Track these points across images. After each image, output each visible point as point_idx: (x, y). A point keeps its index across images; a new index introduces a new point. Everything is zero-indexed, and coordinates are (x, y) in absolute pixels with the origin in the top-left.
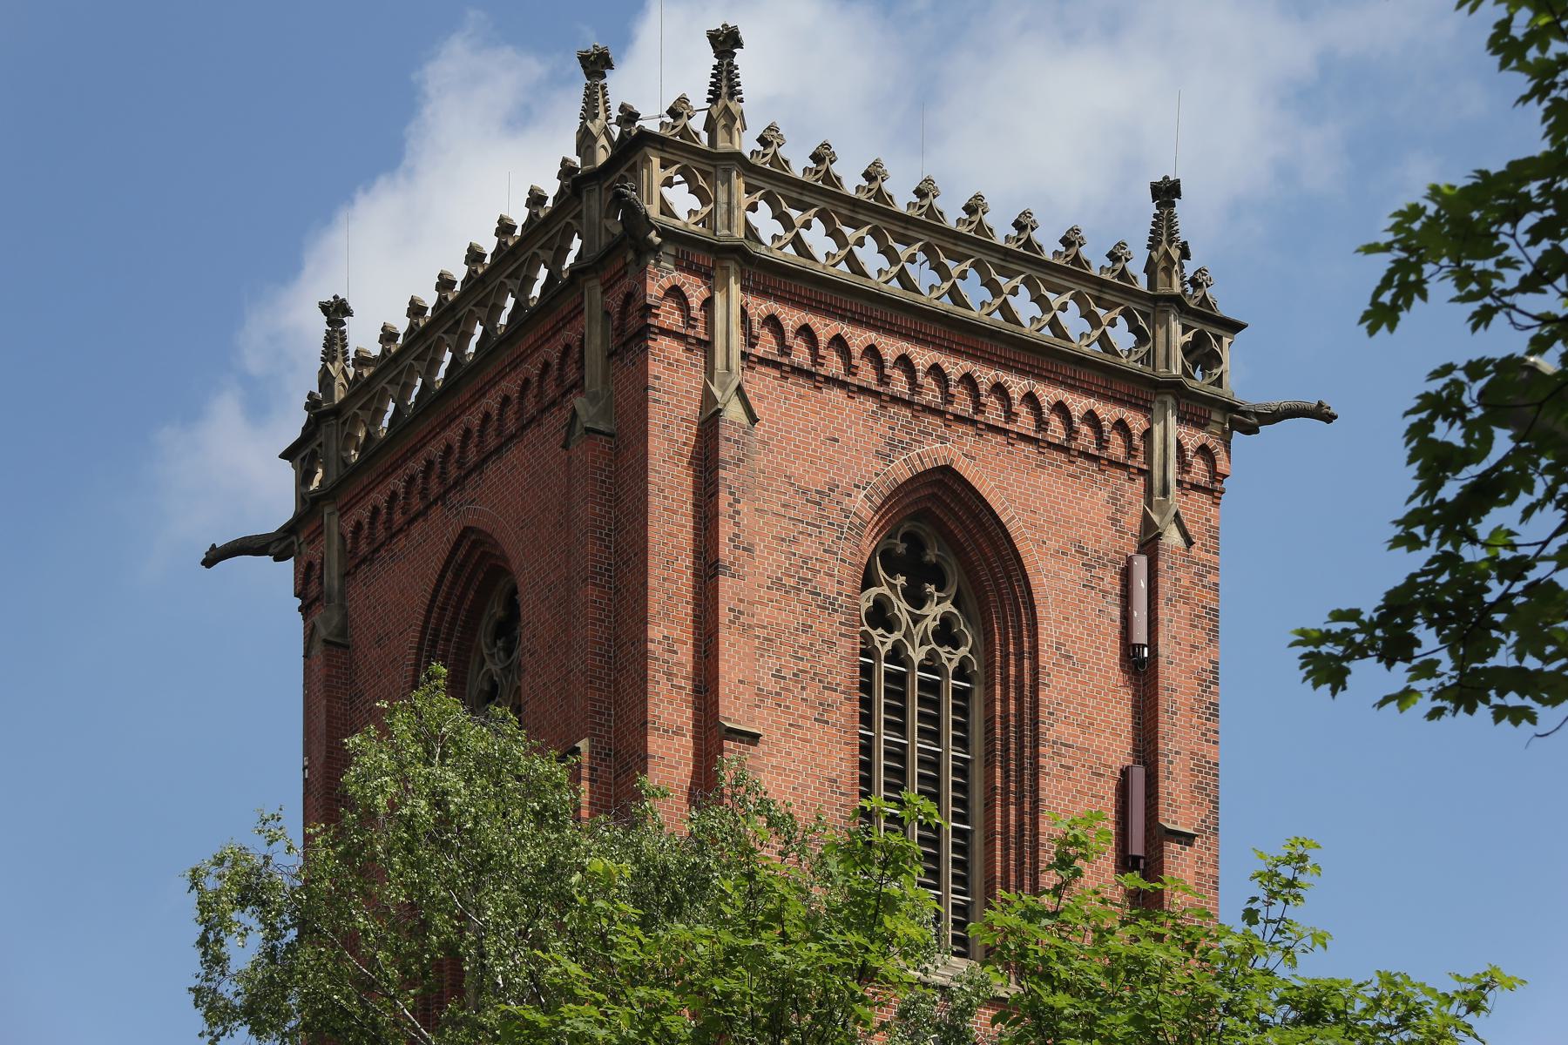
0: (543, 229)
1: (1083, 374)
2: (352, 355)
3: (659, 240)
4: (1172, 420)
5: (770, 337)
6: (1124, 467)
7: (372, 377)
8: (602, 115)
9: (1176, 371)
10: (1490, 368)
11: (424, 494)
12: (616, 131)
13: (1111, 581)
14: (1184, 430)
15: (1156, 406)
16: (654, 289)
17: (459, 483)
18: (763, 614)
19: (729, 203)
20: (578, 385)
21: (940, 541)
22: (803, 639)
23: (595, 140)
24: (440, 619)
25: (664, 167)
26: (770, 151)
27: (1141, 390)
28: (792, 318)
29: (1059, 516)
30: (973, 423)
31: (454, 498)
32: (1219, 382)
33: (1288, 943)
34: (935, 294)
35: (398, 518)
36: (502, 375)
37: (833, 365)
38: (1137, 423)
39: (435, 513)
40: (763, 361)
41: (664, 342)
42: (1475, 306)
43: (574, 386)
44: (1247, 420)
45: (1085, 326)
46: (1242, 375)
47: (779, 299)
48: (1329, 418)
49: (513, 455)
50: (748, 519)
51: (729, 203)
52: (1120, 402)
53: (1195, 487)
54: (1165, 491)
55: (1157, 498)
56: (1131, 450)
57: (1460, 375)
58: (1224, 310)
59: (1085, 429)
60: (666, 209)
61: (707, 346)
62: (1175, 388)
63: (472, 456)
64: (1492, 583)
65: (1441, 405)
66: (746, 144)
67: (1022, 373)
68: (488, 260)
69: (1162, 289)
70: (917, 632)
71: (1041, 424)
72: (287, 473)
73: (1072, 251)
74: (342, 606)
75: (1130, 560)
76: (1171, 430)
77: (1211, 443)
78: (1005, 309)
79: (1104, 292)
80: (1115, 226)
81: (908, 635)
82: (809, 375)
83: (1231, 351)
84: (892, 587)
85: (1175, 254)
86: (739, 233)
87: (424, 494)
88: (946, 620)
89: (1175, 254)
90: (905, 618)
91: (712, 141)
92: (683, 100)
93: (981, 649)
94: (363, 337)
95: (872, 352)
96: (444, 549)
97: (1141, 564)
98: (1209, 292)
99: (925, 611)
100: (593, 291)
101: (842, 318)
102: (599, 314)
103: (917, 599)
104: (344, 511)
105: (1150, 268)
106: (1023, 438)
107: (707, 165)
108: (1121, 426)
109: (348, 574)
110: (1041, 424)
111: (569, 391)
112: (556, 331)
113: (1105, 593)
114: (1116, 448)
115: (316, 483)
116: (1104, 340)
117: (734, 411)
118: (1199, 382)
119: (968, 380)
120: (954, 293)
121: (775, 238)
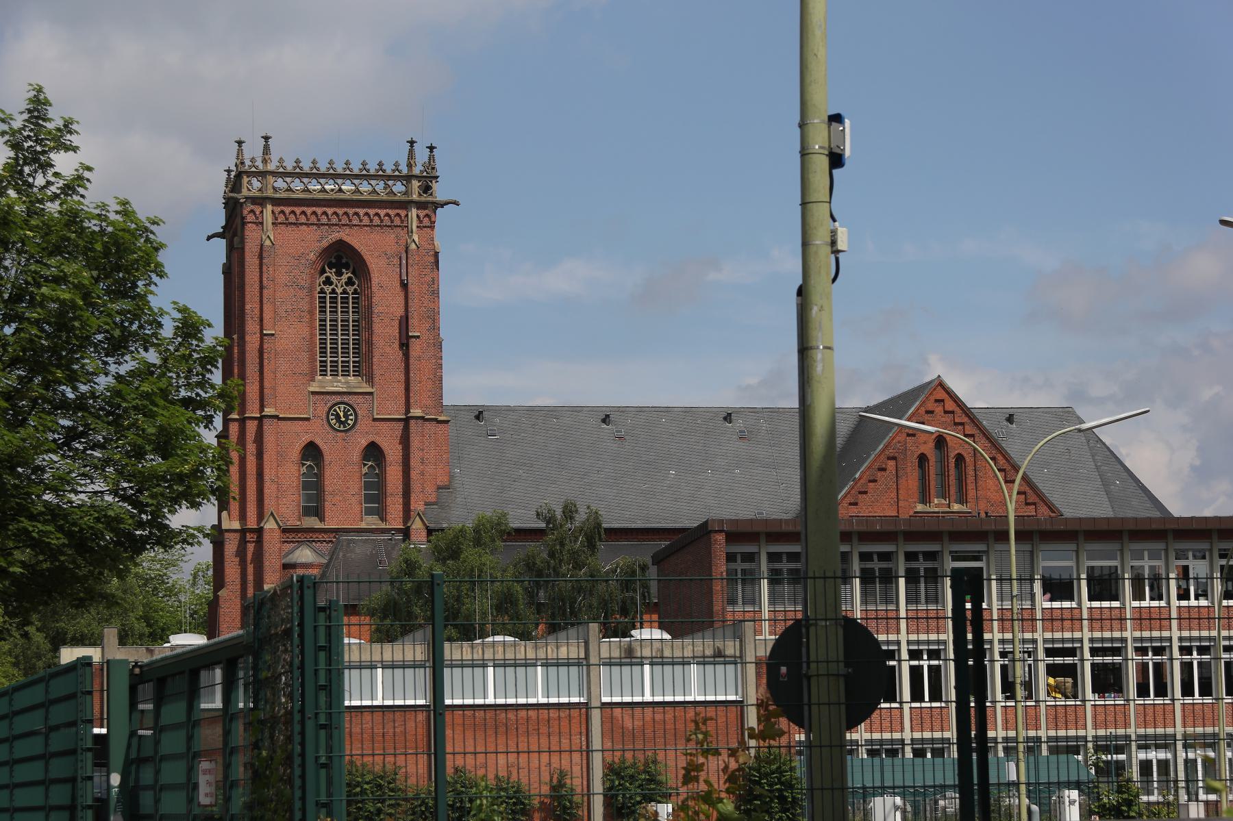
13: (396, 261)
21: (341, 258)
46: (440, 191)
56: (402, 222)
61: (262, 223)
88: (349, 278)
97: (404, 256)
103: (339, 274)
108: (398, 215)
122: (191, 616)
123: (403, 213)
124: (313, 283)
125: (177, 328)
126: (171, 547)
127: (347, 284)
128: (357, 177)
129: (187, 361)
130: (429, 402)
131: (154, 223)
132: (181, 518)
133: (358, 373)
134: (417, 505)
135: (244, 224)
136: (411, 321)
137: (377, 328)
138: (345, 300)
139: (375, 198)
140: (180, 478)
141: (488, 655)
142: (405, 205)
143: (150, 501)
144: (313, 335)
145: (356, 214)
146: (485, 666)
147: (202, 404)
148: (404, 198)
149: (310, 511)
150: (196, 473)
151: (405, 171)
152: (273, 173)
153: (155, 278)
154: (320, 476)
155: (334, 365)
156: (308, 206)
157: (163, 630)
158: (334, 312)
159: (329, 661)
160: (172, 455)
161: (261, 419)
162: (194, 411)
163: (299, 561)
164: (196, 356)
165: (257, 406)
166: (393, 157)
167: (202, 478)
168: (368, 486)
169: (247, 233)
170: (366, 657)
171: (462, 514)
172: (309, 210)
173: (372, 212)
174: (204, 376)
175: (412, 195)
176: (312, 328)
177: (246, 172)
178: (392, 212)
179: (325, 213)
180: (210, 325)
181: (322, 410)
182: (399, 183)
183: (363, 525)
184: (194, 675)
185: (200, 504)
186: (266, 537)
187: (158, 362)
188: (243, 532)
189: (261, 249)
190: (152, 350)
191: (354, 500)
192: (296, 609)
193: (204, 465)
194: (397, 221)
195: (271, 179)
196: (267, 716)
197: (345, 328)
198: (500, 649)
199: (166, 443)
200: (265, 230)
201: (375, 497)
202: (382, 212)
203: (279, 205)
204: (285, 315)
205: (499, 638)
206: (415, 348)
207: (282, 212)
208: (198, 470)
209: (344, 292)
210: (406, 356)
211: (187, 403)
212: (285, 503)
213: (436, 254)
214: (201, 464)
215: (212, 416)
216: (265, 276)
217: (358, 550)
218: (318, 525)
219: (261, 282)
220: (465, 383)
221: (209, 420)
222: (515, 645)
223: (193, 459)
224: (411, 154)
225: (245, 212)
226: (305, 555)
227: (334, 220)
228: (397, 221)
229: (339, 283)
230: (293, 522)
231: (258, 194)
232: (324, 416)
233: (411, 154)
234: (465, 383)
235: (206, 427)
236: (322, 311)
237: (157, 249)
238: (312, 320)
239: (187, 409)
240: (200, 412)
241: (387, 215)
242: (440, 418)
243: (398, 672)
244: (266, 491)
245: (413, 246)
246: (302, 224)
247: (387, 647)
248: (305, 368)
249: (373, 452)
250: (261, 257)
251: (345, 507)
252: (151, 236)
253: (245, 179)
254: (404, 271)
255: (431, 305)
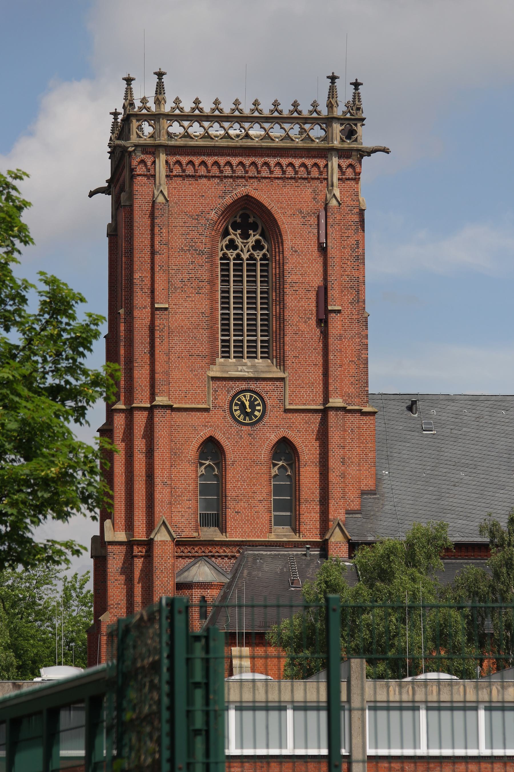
13: (313, 220)
15: (329, 156)
21: (248, 217)
29: (285, 201)
41: (140, 178)
46: (366, 138)
48: (388, 153)
56: (321, 173)
61: (154, 176)
77: (353, 162)
81: (242, 250)
84: (236, 235)
88: (258, 242)
97: (322, 214)
99: (249, 240)
101: (204, 155)
103: (245, 236)
106: (278, 178)
108: (316, 165)
113: (311, 225)
122: (67, 644)
123: (322, 163)
124: (213, 248)
125: (44, 303)
126: (34, 566)
127: (254, 248)
128: (267, 119)
129: (55, 342)
130: (352, 390)
131: (16, 177)
132: (46, 531)
133: (266, 355)
134: (337, 514)
135: (132, 177)
136: (330, 293)
137: (290, 301)
138: (252, 267)
139: (288, 144)
140: (46, 482)
141: (420, 696)
142: (324, 153)
143: (10, 511)
144: (213, 309)
145: (266, 164)
146: (415, 709)
147: (73, 394)
148: (323, 145)
149: (206, 521)
150: (65, 478)
151: (324, 112)
152: (171, 117)
153: (18, 244)
154: (221, 478)
155: (239, 344)
156: (209, 155)
157: (34, 662)
158: (239, 281)
159: (207, 701)
160: (36, 456)
161: (151, 410)
162: (63, 402)
163: (196, 580)
164: (65, 336)
165: (147, 393)
166: (311, 95)
167: (72, 483)
168: (278, 490)
169: (136, 188)
170: (273, 696)
171: (392, 526)
172: (209, 161)
173: (284, 161)
174: (75, 360)
175: (331, 140)
176: (213, 300)
177: (136, 115)
178: (309, 162)
179: (229, 163)
180: (82, 300)
181: (224, 399)
182: (317, 127)
183: (272, 538)
184: (53, 715)
185: (68, 514)
186: (157, 551)
187: (21, 344)
188: (130, 544)
189: (153, 206)
190: (14, 330)
191: (261, 508)
192: (165, 638)
193: (74, 468)
194: (315, 173)
195: (165, 123)
196: (132, 766)
197: (252, 301)
198: (435, 689)
199: (29, 440)
200: (157, 183)
201: (287, 504)
202: (297, 162)
203: (175, 154)
204: (180, 285)
205: (432, 676)
206: (336, 324)
207: (178, 162)
208: (66, 474)
209: (251, 258)
210: (325, 335)
211: (54, 392)
212: (179, 511)
213: (361, 212)
214: (70, 467)
215: (84, 408)
216: (157, 239)
217: (266, 568)
218: (219, 537)
219: (152, 246)
220: (393, 368)
221: (80, 413)
222: (450, 684)
223: (60, 460)
224: (332, 92)
225: (134, 163)
226: (202, 572)
227: (240, 171)
228: (315, 173)
229: (245, 247)
230: (189, 533)
231: (150, 141)
232: (226, 407)
233: (332, 92)
234: (393, 368)
235: (77, 420)
236: (225, 280)
237: (20, 209)
238: (212, 292)
239: (54, 400)
240: (70, 403)
241: (303, 165)
242: (365, 409)
243: (446, 715)
244: (158, 496)
245: (334, 202)
246: (201, 177)
247: (299, 685)
248: (204, 348)
249: (285, 449)
250: (152, 216)
251: (251, 516)
252: (13, 193)
253: (135, 124)
254: (322, 232)
255: (355, 273)
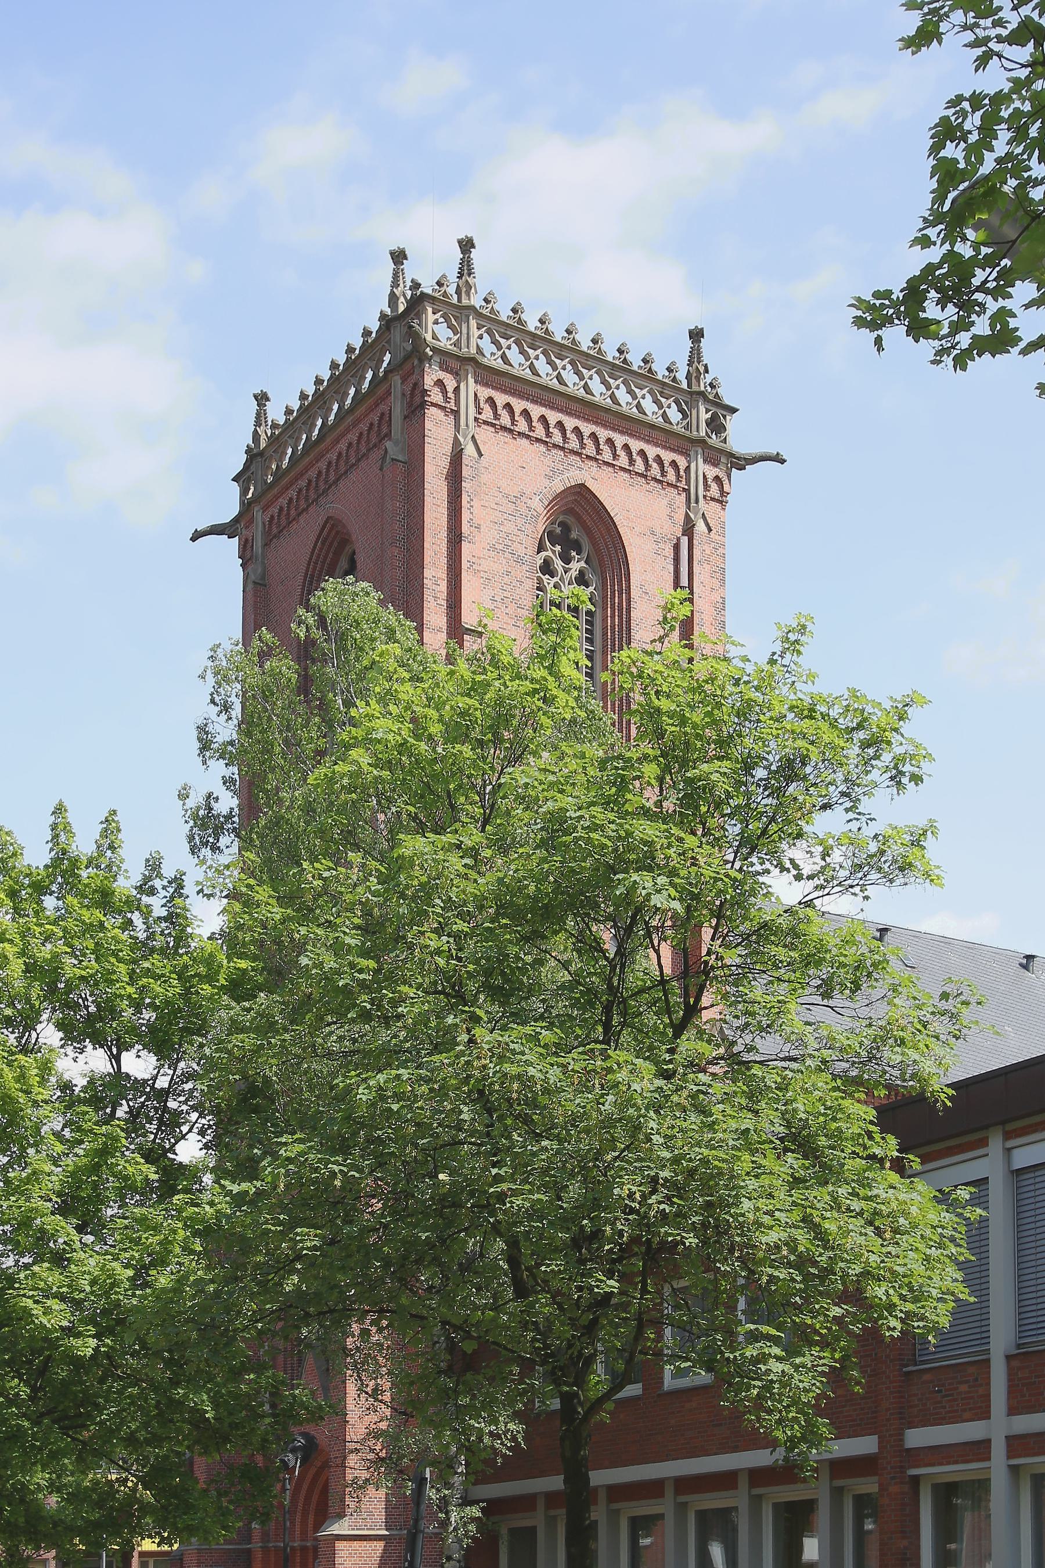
0: (371, 349)
1: (655, 433)
2: (270, 423)
3: (431, 353)
4: (700, 460)
5: (489, 409)
6: (676, 487)
7: (280, 434)
8: (402, 285)
9: (703, 433)
10: (987, 101)
11: (307, 498)
12: (409, 294)
13: (669, 552)
14: (707, 467)
16: (429, 381)
17: (325, 492)
18: (485, 565)
19: (468, 334)
20: (388, 435)
21: (580, 529)
22: (506, 579)
23: (398, 299)
24: (314, 569)
25: (434, 313)
26: (490, 306)
27: (684, 444)
28: (501, 399)
29: (641, 513)
30: (596, 460)
31: (322, 500)
32: (725, 441)
33: (794, 679)
34: (576, 388)
35: (293, 512)
36: (347, 430)
37: (522, 426)
38: (682, 462)
39: (311, 510)
40: (485, 423)
41: (433, 410)
42: (979, 51)
43: (386, 435)
44: (740, 462)
45: (655, 408)
46: (739, 436)
47: (494, 388)
49: (353, 476)
50: (475, 511)
51: (468, 334)
52: (673, 450)
53: (713, 499)
54: (697, 502)
55: (693, 505)
56: (678, 476)
57: (966, 105)
58: (727, 401)
59: (655, 465)
60: (435, 337)
61: (456, 413)
62: (702, 442)
63: (332, 477)
64: (978, 271)
65: (946, 132)
66: (477, 301)
67: (622, 433)
68: (341, 368)
69: (695, 388)
70: (567, 578)
71: (632, 462)
72: (236, 488)
73: (648, 366)
74: (263, 563)
75: (678, 539)
76: (702, 468)
78: (613, 397)
79: (664, 389)
80: (670, 355)
82: (511, 431)
83: (732, 423)
84: (554, 552)
85: (702, 369)
86: (473, 350)
87: (307, 498)
88: (581, 572)
89: (702, 369)
90: (560, 570)
91: (459, 300)
92: (444, 276)
93: (600, 588)
94: (276, 413)
95: (543, 419)
96: (317, 529)
98: (719, 390)
100: (396, 379)
102: (400, 396)
103: (566, 559)
104: (265, 509)
105: (688, 377)
107: (459, 314)
108: (674, 464)
109: (266, 545)
110: (632, 462)
111: (383, 438)
112: (377, 405)
114: (671, 476)
115: (250, 495)
116: (664, 415)
117: (470, 450)
118: (714, 440)
119: (594, 436)
120: (586, 387)
121: (493, 354)
